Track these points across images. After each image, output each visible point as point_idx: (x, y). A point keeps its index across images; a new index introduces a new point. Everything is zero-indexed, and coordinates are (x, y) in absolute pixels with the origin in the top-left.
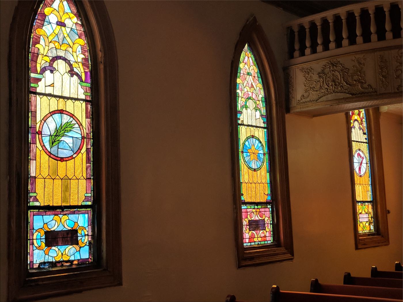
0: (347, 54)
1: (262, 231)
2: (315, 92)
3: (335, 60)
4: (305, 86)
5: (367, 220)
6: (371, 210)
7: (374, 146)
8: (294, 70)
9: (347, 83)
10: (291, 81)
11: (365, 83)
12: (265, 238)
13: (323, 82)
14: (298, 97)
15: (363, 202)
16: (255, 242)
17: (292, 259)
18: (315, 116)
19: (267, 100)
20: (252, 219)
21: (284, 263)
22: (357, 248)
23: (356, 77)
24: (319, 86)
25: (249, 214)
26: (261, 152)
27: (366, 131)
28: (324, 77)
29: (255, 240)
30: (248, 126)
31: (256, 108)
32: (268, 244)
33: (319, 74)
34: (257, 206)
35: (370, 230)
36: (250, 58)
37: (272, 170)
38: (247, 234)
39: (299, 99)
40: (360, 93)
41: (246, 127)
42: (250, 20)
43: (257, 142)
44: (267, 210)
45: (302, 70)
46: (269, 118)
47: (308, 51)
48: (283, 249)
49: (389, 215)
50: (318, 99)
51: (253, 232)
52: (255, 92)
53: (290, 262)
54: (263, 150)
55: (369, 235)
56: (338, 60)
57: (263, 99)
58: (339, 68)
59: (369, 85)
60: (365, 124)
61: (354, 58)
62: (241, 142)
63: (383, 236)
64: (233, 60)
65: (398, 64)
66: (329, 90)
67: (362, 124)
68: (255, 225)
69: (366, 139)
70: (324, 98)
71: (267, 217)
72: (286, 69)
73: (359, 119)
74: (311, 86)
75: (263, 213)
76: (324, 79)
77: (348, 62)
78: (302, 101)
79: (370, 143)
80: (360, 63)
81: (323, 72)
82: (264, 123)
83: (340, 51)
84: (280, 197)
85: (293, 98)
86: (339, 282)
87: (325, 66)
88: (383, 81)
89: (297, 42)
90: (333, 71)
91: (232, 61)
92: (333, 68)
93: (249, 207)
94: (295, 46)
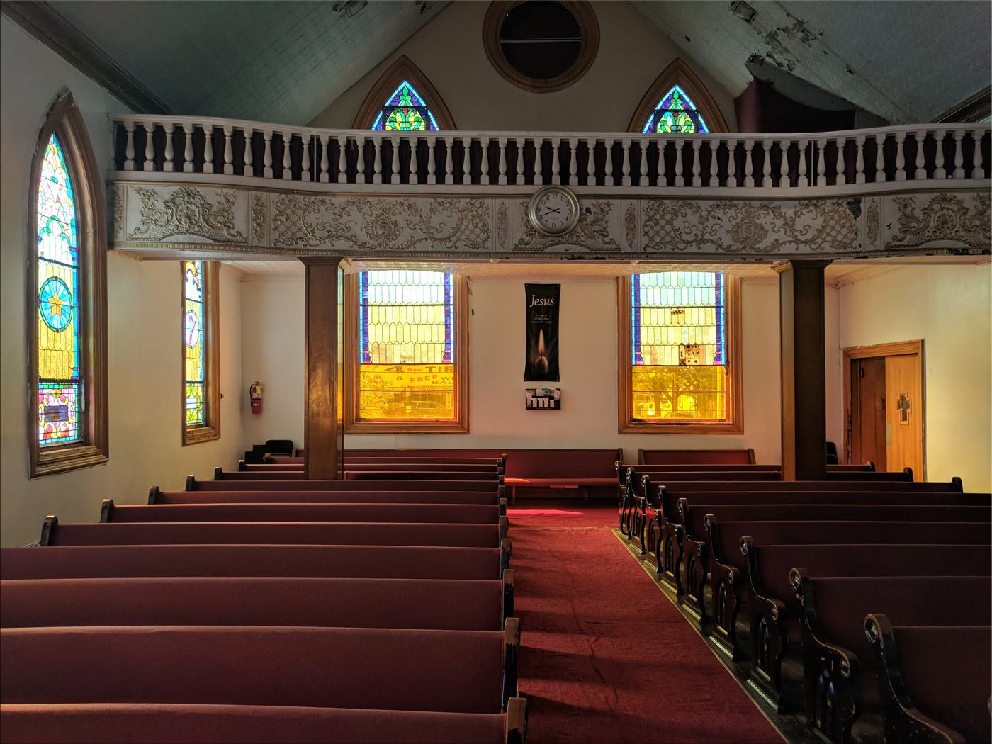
0: (211, 185)
1: (63, 422)
2: (159, 227)
3: (191, 188)
4: (142, 214)
5: (195, 406)
6: (200, 393)
7: (210, 308)
8: (125, 188)
9: (207, 224)
10: (118, 203)
11: (233, 228)
12: (67, 433)
13: (172, 215)
14: (131, 229)
15: (194, 382)
16: (52, 439)
17: (105, 462)
18: (144, 259)
19: (80, 226)
20: (50, 405)
21: (94, 468)
22: (184, 444)
23: (220, 219)
24: (165, 219)
25: (49, 397)
26: (68, 303)
27: (200, 286)
28: (174, 209)
29: (53, 435)
30: (50, 261)
31: (62, 235)
32: (71, 442)
33: (166, 202)
34: (59, 384)
35: (198, 419)
36: (56, 155)
37: (82, 332)
38: (42, 427)
39: (132, 232)
40: (225, 241)
41: (47, 263)
42: (63, 97)
43: (63, 287)
44: (72, 391)
45: (138, 191)
46: (80, 252)
47: (149, 165)
48: (93, 449)
49: (222, 400)
50: (163, 238)
51: (51, 424)
52: (62, 210)
53: (102, 466)
54: (71, 301)
55: (196, 427)
56: (198, 189)
57: (74, 224)
58: (198, 201)
59: (238, 232)
60: (200, 277)
61: (220, 192)
62: (40, 286)
63: (213, 428)
64: (36, 154)
65: (278, 212)
66: (180, 228)
67: (196, 276)
68: (56, 414)
69: (200, 297)
70: (172, 239)
71: (71, 397)
72: (110, 183)
73: (194, 270)
74: (152, 217)
75: (66, 395)
76: (175, 211)
77: (212, 196)
78: (135, 236)
79: (205, 303)
80: (228, 201)
81: (173, 200)
82: (73, 259)
83: (198, 177)
84: (93, 373)
85: (121, 228)
86: (181, 489)
87: (177, 193)
88: (256, 231)
89: (131, 148)
90: (188, 203)
91: (34, 156)
92: (188, 198)
93: (47, 387)
94: (127, 154)
